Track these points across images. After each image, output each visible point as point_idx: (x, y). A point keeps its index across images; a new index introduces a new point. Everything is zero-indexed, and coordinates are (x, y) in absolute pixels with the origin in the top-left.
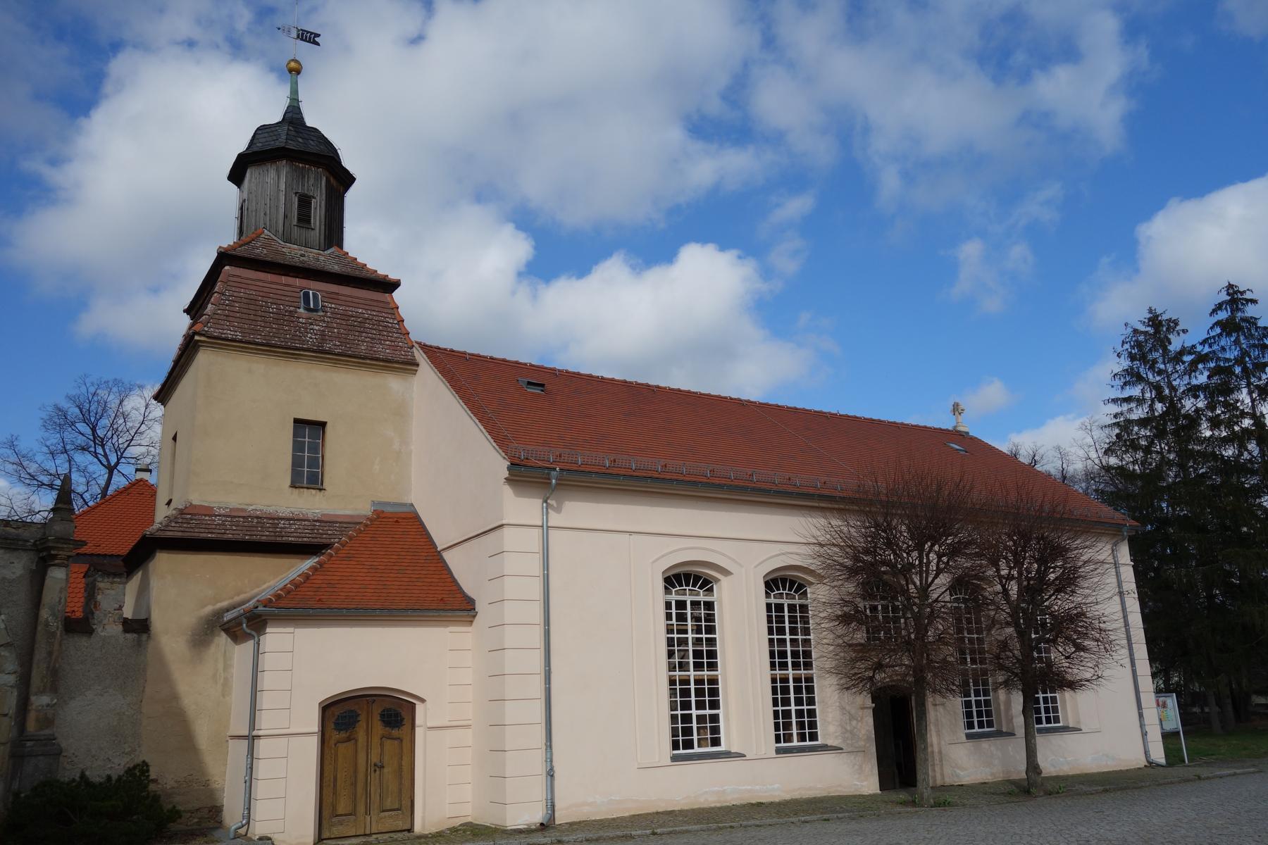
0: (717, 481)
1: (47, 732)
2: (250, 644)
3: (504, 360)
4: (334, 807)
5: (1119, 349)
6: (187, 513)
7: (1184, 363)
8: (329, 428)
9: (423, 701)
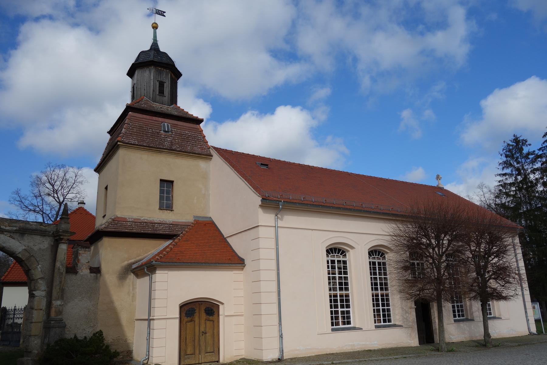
0: (348, 207)
1: (60, 317)
2: (147, 279)
3: (248, 154)
4: (186, 351)
5: (502, 152)
6: (116, 220)
7: (529, 158)
8: (175, 183)
9: (222, 304)
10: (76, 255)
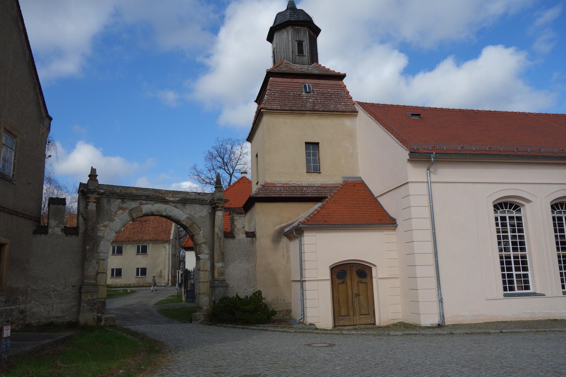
1: (222, 277)
2: (297, 242)
4: (340, 312)
6: (266, 186)
8: (320, 145)
9: (375, 266)
10: (232, 221)
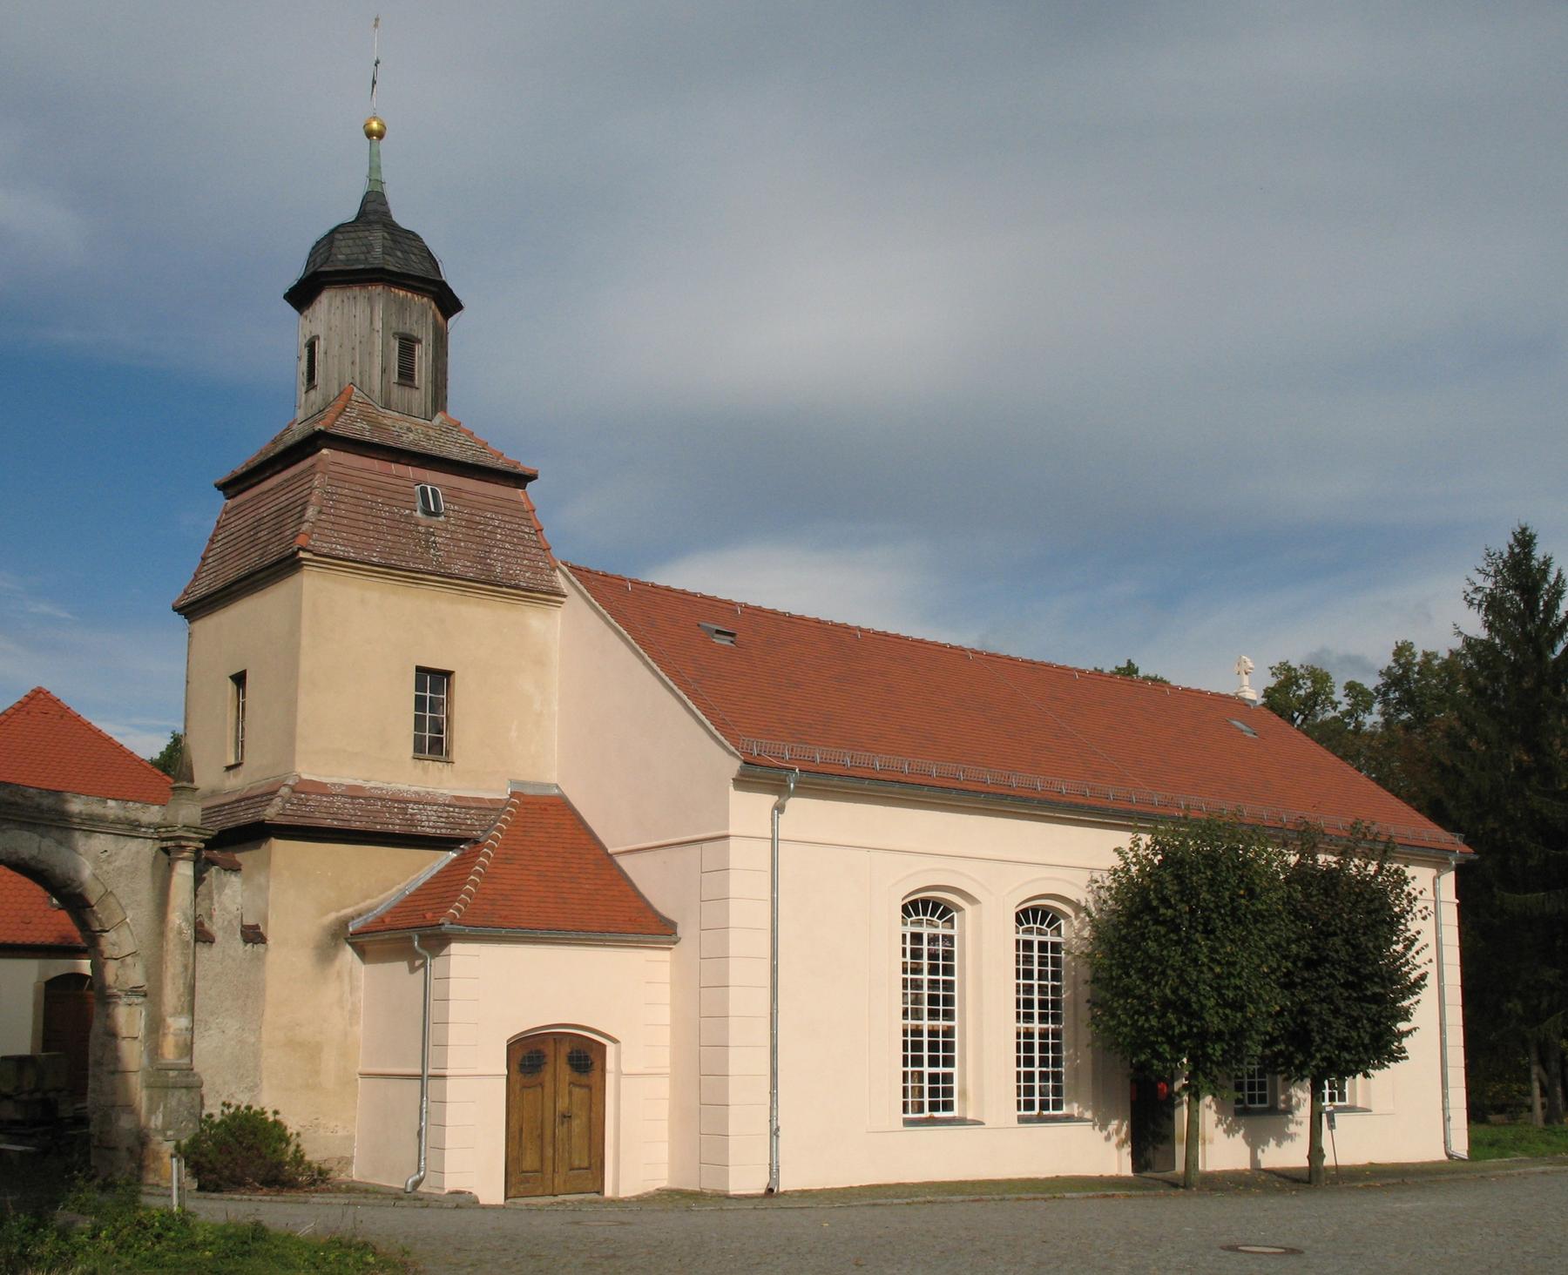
8: (458, 683)
9: (615, 1041)
